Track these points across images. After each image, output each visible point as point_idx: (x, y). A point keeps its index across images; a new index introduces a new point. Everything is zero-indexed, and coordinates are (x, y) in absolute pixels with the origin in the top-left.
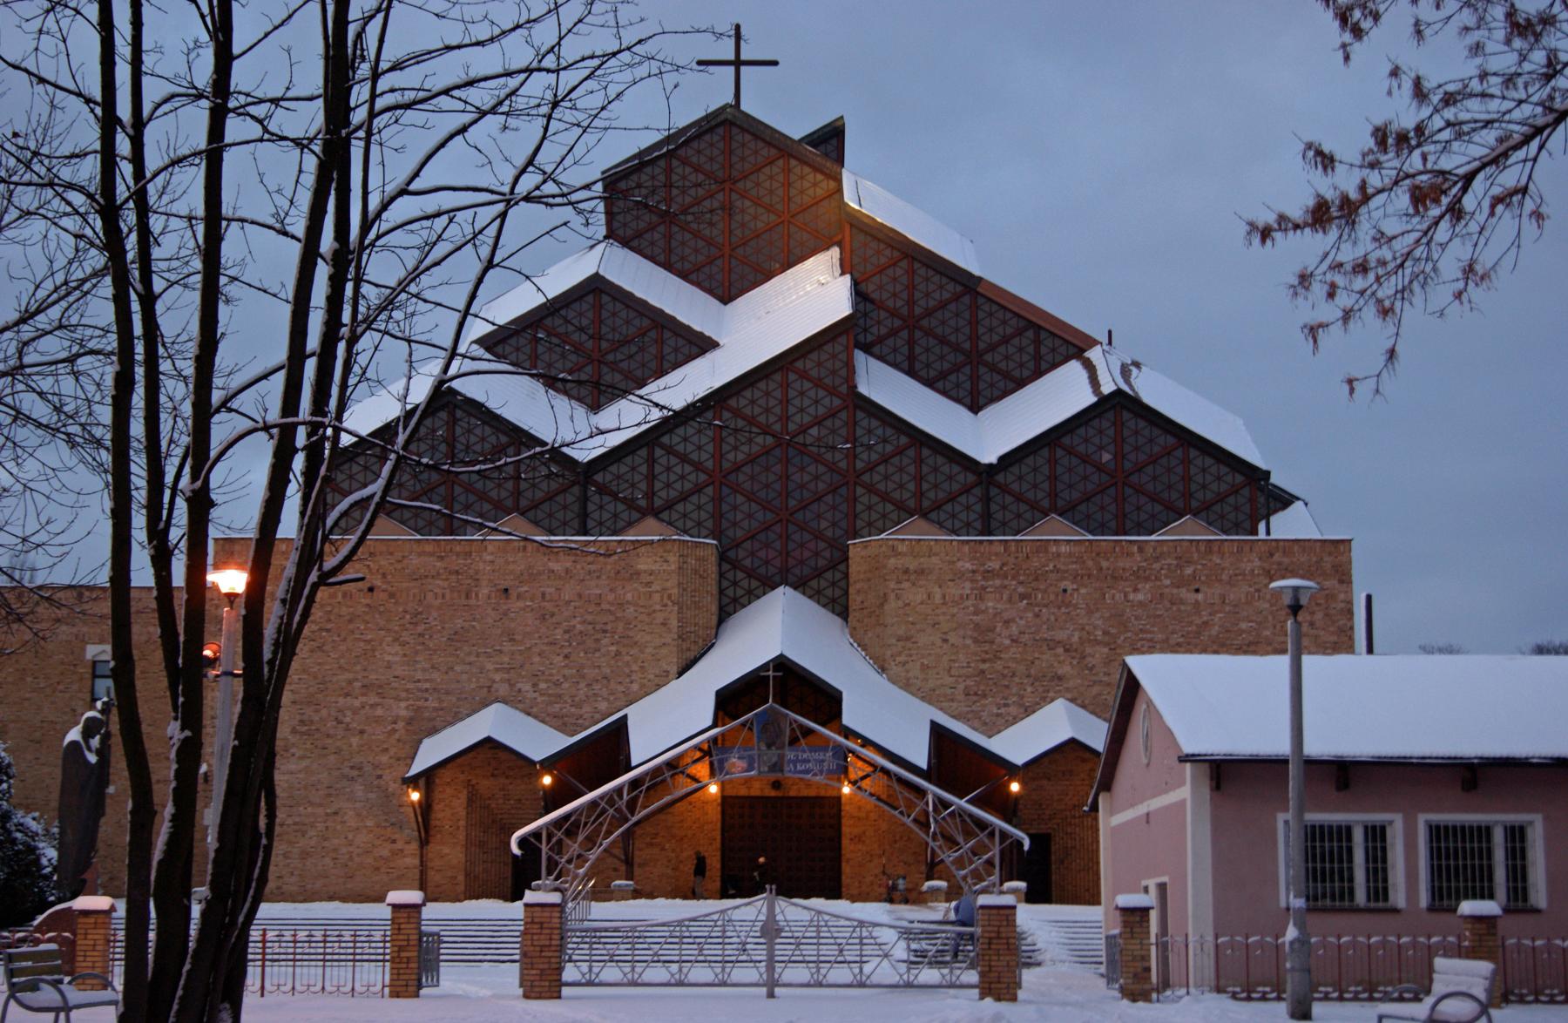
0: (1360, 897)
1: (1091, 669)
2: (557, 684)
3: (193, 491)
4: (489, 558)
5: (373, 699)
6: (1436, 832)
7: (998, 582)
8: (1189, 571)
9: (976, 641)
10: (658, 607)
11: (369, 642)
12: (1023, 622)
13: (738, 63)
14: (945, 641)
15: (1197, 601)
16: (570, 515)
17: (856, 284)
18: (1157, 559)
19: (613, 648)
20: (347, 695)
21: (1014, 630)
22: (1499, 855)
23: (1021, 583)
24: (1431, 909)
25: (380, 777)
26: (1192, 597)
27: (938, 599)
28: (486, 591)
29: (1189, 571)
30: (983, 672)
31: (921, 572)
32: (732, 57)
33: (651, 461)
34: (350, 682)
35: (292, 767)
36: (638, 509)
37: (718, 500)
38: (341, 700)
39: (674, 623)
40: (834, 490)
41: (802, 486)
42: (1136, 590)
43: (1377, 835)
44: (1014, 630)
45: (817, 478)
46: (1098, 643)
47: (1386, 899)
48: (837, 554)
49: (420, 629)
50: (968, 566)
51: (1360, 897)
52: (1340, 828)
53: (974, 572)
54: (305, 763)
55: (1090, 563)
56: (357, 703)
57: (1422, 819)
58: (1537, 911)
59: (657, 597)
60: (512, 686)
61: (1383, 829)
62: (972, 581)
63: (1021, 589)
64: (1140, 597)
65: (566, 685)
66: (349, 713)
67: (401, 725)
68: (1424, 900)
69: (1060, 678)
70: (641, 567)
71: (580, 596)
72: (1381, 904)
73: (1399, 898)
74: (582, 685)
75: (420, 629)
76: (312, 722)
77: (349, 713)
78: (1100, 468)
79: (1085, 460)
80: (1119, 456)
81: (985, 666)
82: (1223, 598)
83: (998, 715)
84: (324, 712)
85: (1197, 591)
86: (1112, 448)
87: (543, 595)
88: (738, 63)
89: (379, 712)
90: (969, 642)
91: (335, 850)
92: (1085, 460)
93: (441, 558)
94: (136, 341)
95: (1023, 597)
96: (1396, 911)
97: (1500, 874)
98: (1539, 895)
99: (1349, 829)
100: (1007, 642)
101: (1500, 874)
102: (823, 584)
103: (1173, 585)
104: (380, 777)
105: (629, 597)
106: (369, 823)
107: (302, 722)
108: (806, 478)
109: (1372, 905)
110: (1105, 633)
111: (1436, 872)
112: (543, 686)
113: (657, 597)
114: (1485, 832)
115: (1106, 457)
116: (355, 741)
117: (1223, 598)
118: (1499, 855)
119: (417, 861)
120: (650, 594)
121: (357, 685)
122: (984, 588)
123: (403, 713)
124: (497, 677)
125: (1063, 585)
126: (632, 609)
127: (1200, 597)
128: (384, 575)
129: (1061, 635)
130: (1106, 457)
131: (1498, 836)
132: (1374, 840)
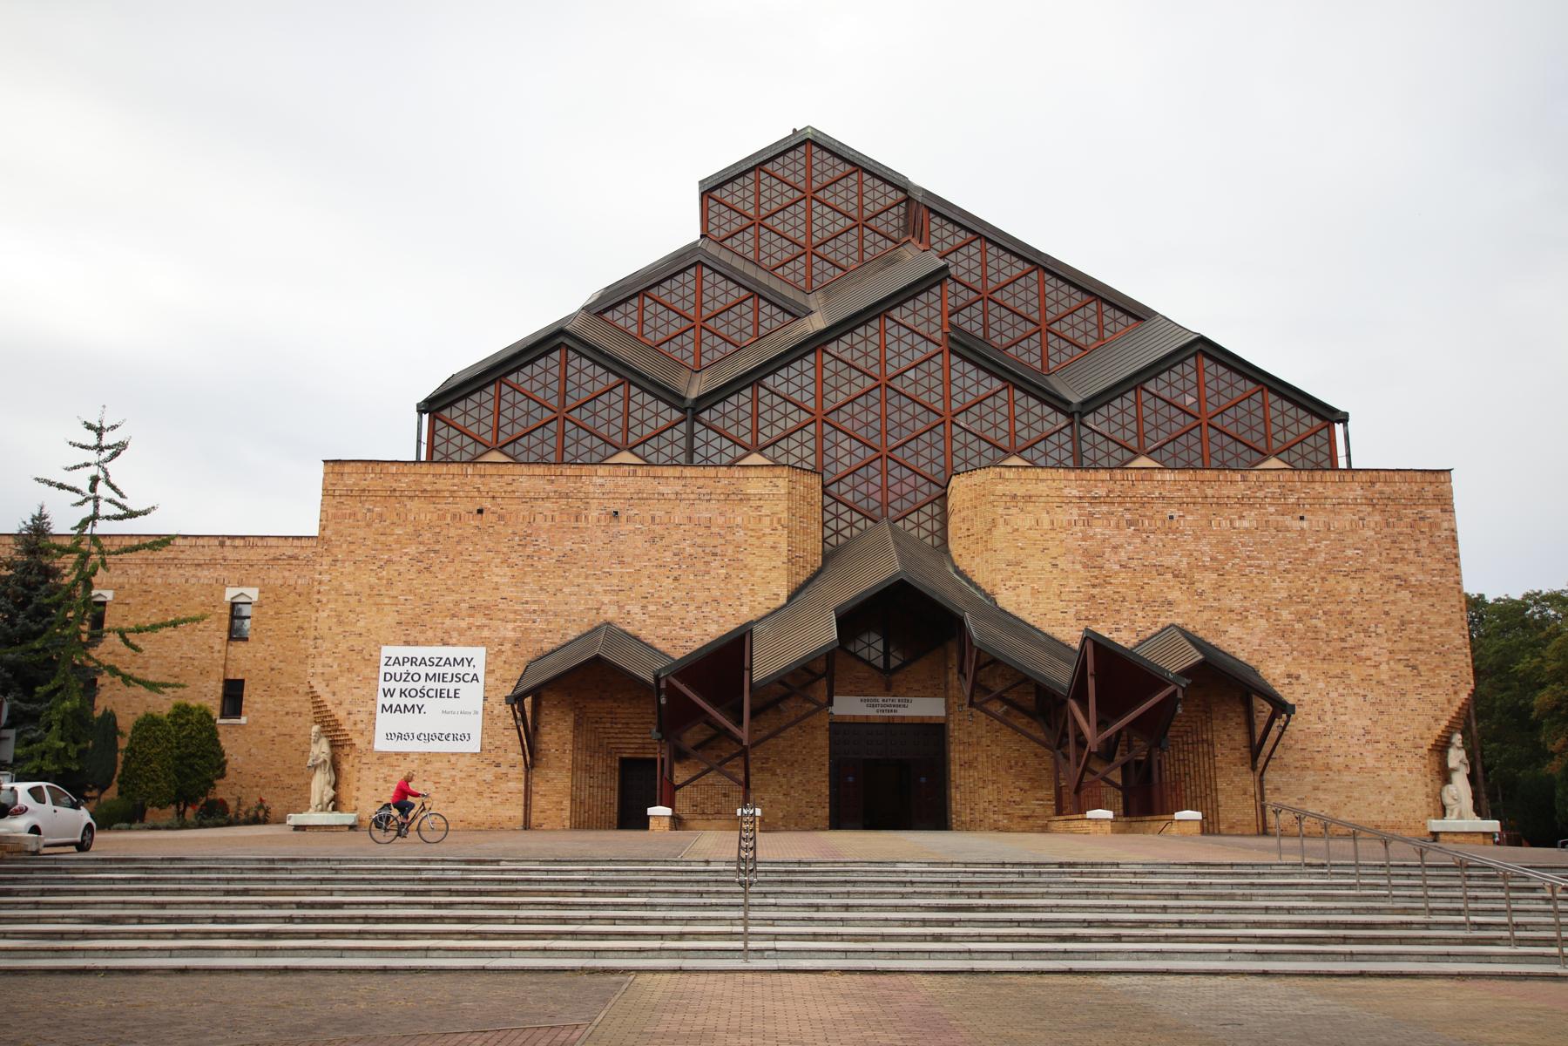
2: (667, 606)
7: (1105, 508)
9: (1085, 566)
10: (768, 531)
14: (1055, 565)
15: (1302, 529)
20: (453, 616)
26: (1297, 524)
27: (1046, 525)
28: (595, 514)
31: (1028, 498)
34: (457, 603)
38: (448, 622)
39: (784, 546)
42: (1241, 517)
44: (1123, 555)
49: (530, 550)
50: (1075, 492)
55: (1195, 491)
56: (463, 624)
59: (767, 521)
60: (621, 607)
63: (1128, 516)
64: (1246, 524)
67: (507, 646)
69: (1170, 603)
74: (692, 608)
75: (530, 550)
81: (1095, 591)
85: (1302, 518)
87: (653, 518)
90: (1078, 567)
91: (437, 774)
95: (1130, 523)
100: (1117, 567)
105: (739, 520)
108: (905, 417)
112: (652, 608)
113: (767, 521)
115: (1190, 400)
119: (521, 786)
121: (464, 606)
122: (1091, 514)
123: (511, 634)
124: (606, 599)
127: (1305, 524)
129: (1169, 561)
130: (1190, 400)
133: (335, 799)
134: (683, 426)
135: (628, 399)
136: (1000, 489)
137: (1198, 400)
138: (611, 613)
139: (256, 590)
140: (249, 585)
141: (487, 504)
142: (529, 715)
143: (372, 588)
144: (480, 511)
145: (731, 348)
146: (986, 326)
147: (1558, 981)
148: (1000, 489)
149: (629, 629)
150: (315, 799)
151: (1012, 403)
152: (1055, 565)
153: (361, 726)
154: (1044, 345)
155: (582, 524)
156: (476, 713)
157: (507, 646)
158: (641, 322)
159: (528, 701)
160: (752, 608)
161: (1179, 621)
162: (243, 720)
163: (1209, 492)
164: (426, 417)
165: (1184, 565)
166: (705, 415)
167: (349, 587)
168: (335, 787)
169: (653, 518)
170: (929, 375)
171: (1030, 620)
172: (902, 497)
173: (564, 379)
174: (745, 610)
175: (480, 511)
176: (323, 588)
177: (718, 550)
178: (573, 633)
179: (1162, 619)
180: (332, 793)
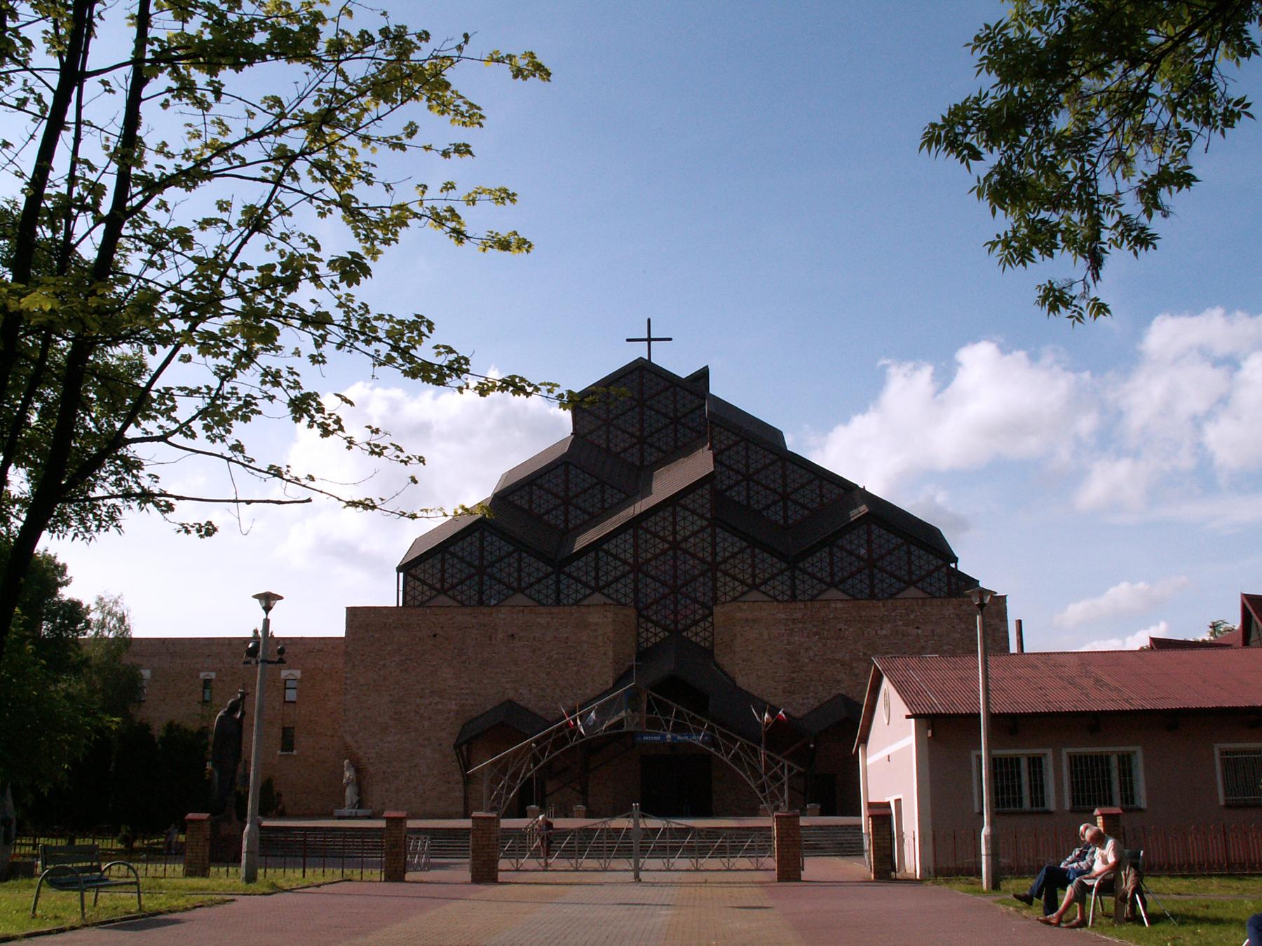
0: (1026, 804)
1: (856, 676)
2: (543, 690)
3: (181, 309)
4: (503, 616)
5: (436, 699)
6: (1075, 761)
7: (801, 625)
8: (912, 617)
9: (788, 660)
10: (601, 644)
11: (434, 666)
12: (816, 649)
13: (649, 340)
14: (771, 661)
15: (918, 635)
16: (550, 592)
17: (715, 456)
18: (894, 610)
19: (575, 668)
20: (421, 697)
21: (811, 653)
22: (1115, 774)
23: (814, 626)
24: (1072, 811)
25: (441, 745)
26: (915, 631)
27: (766, 636)
28: (500, 636)
29: (912, 617)
30: (793, 679)
31: (755, 621)
32: (646, 337)
33: (597, 559)
34: (423, 689)
35: (389, 739)
36: (590, 587)
37: (636, 581)
38: (418, 700)
39: (611, 654)
40: (703, 574)
41: (685, 572)
42: (882, 629)
43: (1036, 763)
44: (811, 653)
45: (694, 567)
46: (860, 659)
47: (1043, 805)
48: (707, 612)
49: (464, 658)
50: (783, 616)
51: (1026, 804)
52: (1012, 759)
53: (787, 619)
54: (398, 736)
55: (854, 614)
56: (427, 702)
57: (1065, 752)
58: (1141, 810)
59: (600, 638)
60: (516, 691)
61: (1040, 759)
62: (785, 625)
63: (814, 630)
64: (884, 632)
65: (548, 691)
66: (423, 708)
67: (452, 714)
68: (1067, 805)
69: (839, 681)
70: (591, 620)
71: (555, 638)
72: (1040, 809)
73: (1051, 804)
74: (558, 690)
75: (464, 658)
76: (401, 713)
77: (423, 708)
78: (859, 558)
79: (851, 553)
80: (870, 551)
81: (794, 675)
82: (933, 631)
83: (803, 704)
84: (409, 707)
85: (918, 628)
86: (865, 546)
87: (534, 639)
88: (649, 340)
89: (440, 707)
90: (784, 661)
91: (415, 788)
92: (851, 553)
93: (475, 617)
94: (514, 861)
95: (816, 634)
96: (1049, 813)
97: (1116, 787)
98: (1142, 801)
99: (1018, 760)
100: (807, 660)
101: (1116, 787)
102: (699, 629)
103: (904, 625)
104: (441, 745)
105: (584, 638)
106: (435, 772)
107: (396, 713)
108: (688, 567)
109: (1034, 809)
110: (865, 654)
111: (1075, 787)
112: (534, 691)
113: (600, 638)
114: (1105, 759)
115: (863, 551)
116: (426, 724)
117: (933, 631)
118: (1115, 774)
119: (462, 794)
120: (596, 637)
121: (428, 691)
122: (792, 629)
123: (454, 707)
124: (508, 686)
125: (839, 626)
126: (586, 646)
127: (919, 631)
128: (442, 628)
129: (838, 656)
130: (863, 551)
131: (1114, 761)
132: (1035, 766)
133: (359, 801)
134: (553, 577)
135: (520, 560)
136: (739, 615)
137: (868, 551)
138: (511, 694)
139: (299, 672)
140: (295, 669)
141: (439, 631)
142: (465, 753)
143: (375, 681)
144: (435, 636)
145: (587, 517)
146: (748, 497)
147: (1221, 927)
148: (739, 615)
149: (522, 704)
150: (348, 802)
151: (753, 556)
152: (771, 661)
153: (372, 761)
154: (785, 509)
155: (493, 642)
156: (22, 175)
157: (452, 714)
158: (530, 501)
159: (464, 748)
160: (593, 690)
161: (843, 692)
162: (295, 752)
163: (863, 613)
164: (401, 575)
165: (847, 658)
166: (567, 569)
167: (362, 681)
168: (359, 795)
169: (534, 639)
170: (703, 540)
171: (756, 693)
172: (686, 617)
173: (482, 548)
174: (588, 691)
175: (435, 636)
176: (348, 682)
177: (573, 656)
178: (489, 707)
179: (834, 691)
180: (357, 798)
